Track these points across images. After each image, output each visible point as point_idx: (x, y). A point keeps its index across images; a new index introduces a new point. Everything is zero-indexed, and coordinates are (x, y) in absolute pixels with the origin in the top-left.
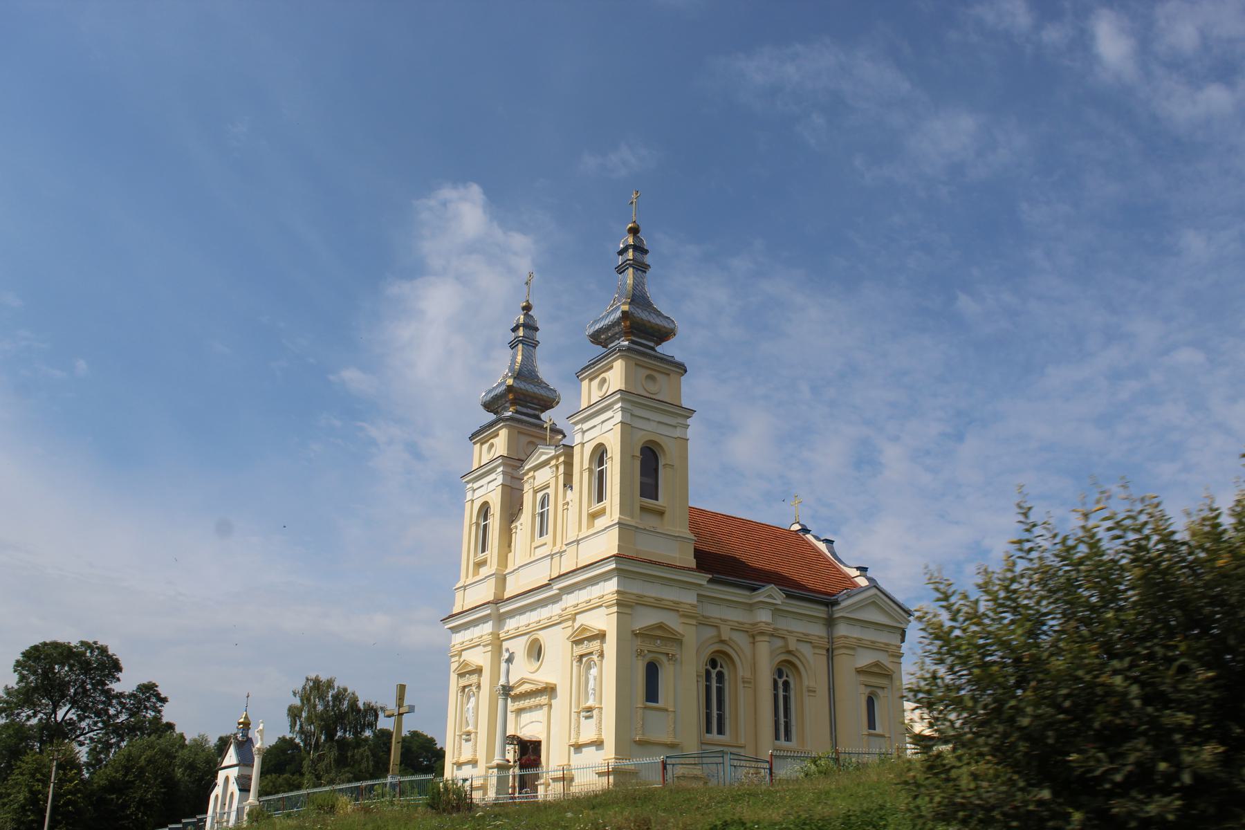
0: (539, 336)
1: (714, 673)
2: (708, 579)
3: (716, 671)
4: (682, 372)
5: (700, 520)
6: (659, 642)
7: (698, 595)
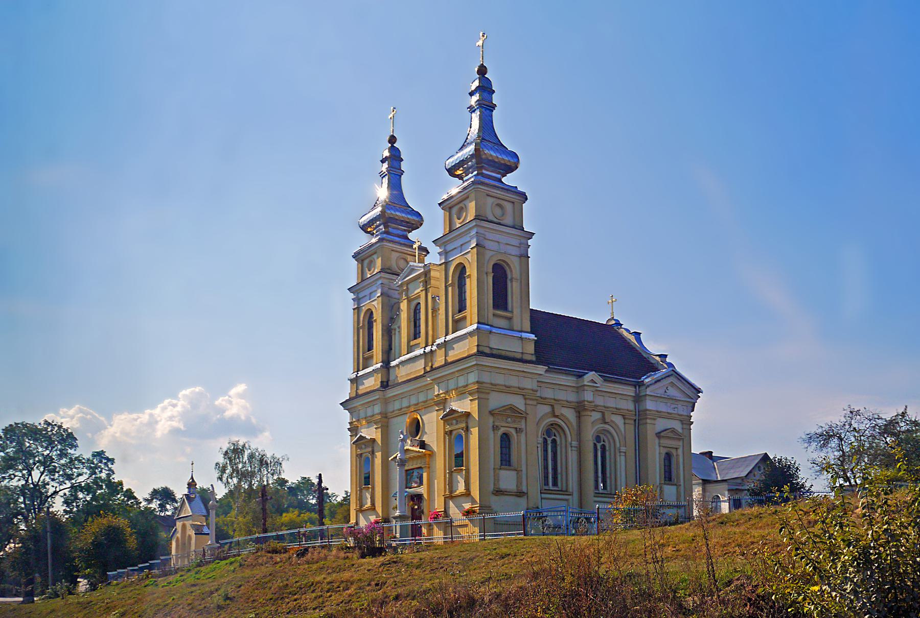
2: (545, 370)
5: (540, 320)
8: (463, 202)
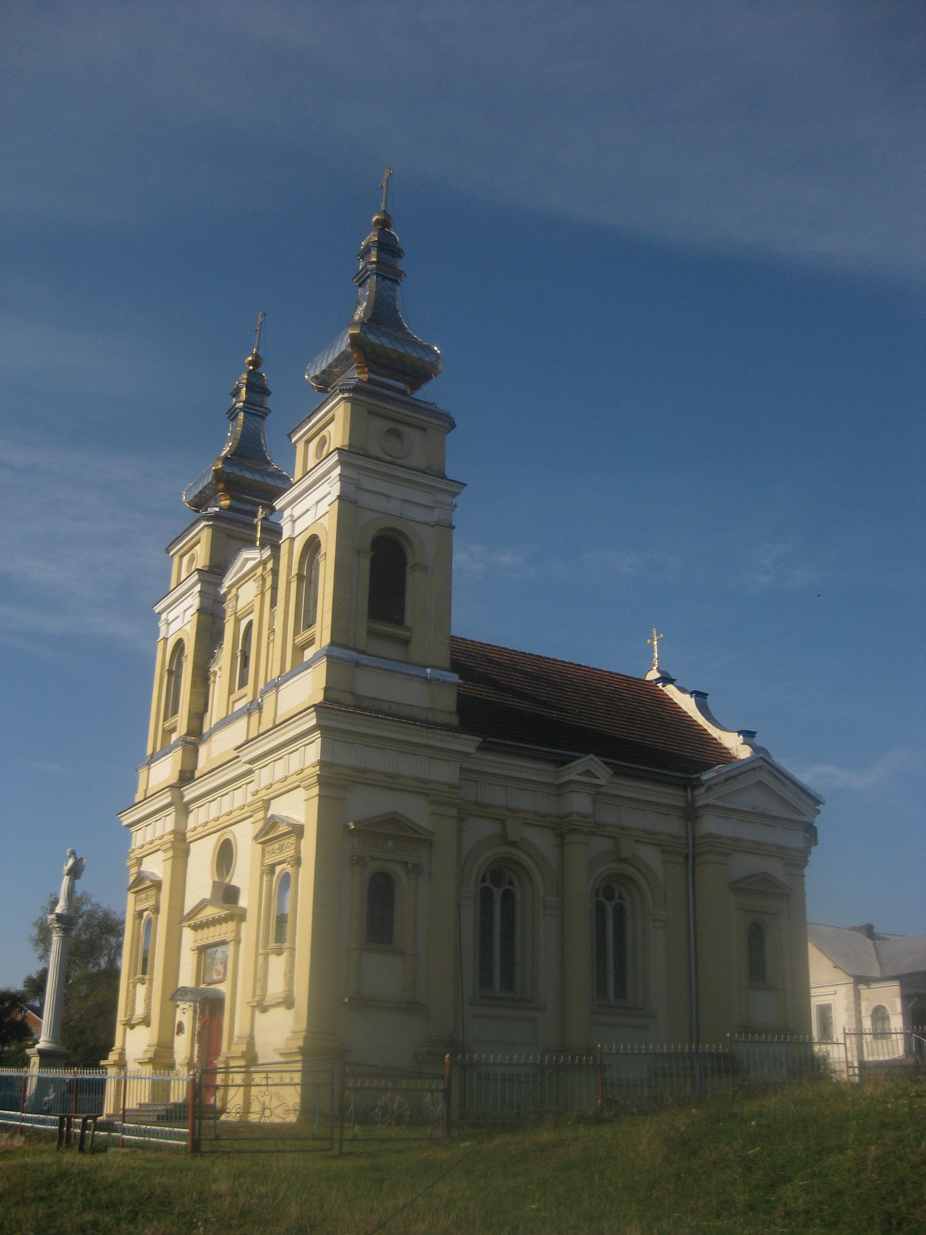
0: (269, 402)
1: (609, 907)
3: (613, 903)
4: (447, 425)
6: (390, 843)
7: (462, 769)
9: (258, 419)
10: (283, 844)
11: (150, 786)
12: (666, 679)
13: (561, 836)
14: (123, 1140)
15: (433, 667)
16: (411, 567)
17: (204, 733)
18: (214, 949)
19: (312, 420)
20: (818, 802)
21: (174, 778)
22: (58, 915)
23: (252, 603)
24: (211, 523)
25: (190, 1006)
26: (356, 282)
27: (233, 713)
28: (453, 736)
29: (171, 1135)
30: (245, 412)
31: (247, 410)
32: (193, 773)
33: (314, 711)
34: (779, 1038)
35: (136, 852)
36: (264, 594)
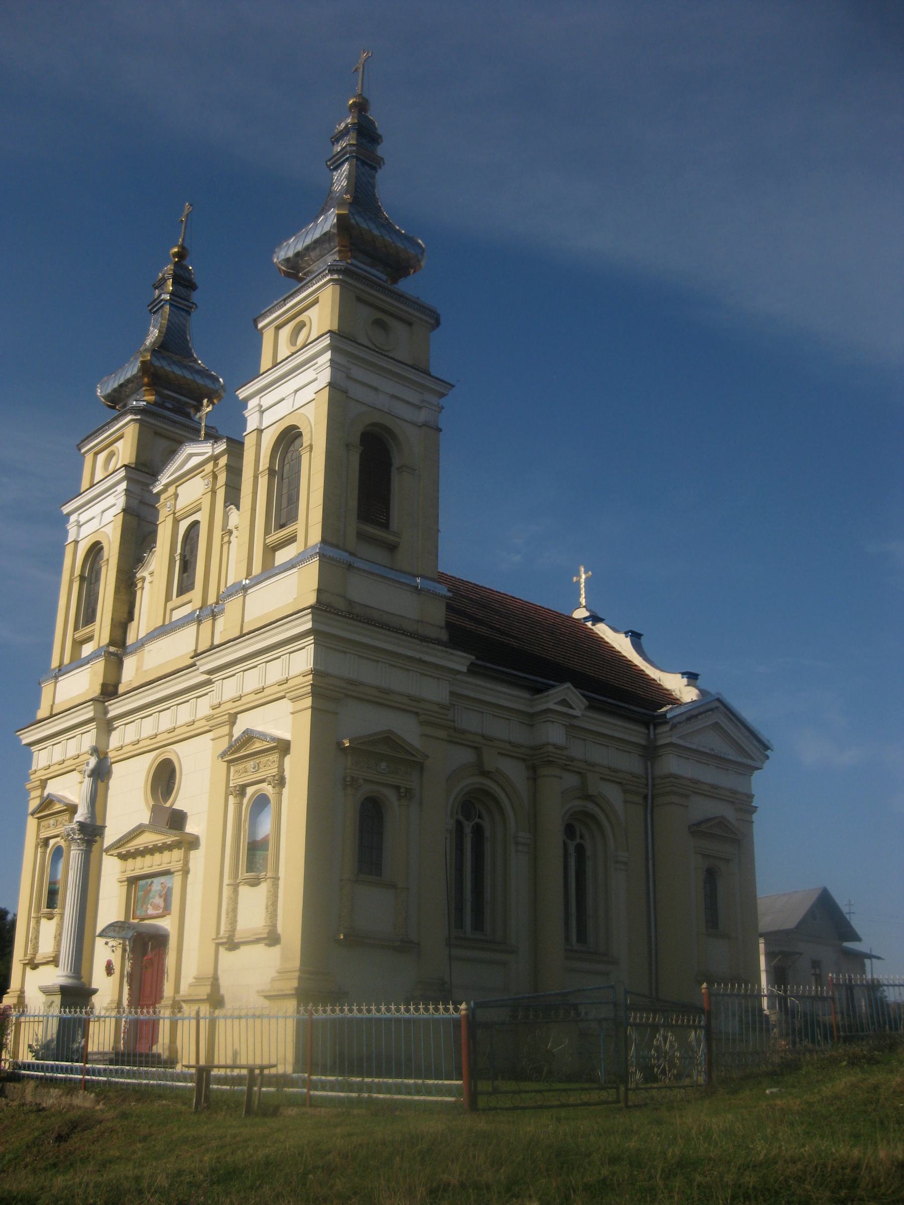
3: (575, 843)
4: (432, 322)
8: (305, 313)
9: (183, 314)
10: (260, 762)
11: (57, 702)
12: (596, 619)
13: (534, 768)
14: (311, 1097)
15: (422, 577)
16: (397, 469)
17: (127, 644)
18: (149, 881)
19: (288, 303)
20: (767, 748)
21: (95, 692)
22: (81, 824)
23: (199, 502)
24: (139, 417)
25: (120, 944)
26: (332, 165)
27: (171, 623)
28: (446, 651)
29: (439, 1091)
30: (171, 305)
31: (172, 302)
32: (116, 686)
33: (309, 613)
34: (726, 989)
35: (38, 774)
36: (216, 493)
